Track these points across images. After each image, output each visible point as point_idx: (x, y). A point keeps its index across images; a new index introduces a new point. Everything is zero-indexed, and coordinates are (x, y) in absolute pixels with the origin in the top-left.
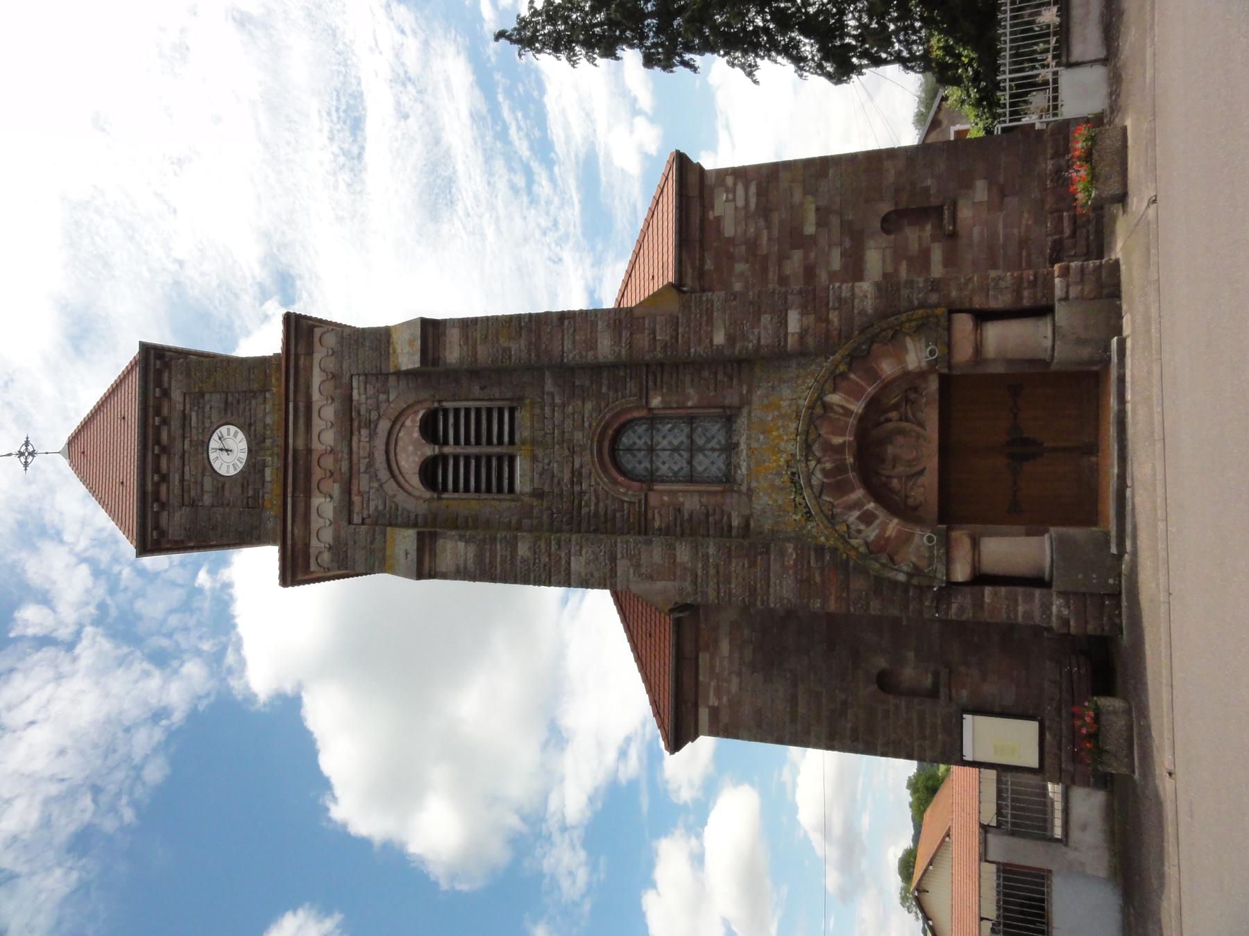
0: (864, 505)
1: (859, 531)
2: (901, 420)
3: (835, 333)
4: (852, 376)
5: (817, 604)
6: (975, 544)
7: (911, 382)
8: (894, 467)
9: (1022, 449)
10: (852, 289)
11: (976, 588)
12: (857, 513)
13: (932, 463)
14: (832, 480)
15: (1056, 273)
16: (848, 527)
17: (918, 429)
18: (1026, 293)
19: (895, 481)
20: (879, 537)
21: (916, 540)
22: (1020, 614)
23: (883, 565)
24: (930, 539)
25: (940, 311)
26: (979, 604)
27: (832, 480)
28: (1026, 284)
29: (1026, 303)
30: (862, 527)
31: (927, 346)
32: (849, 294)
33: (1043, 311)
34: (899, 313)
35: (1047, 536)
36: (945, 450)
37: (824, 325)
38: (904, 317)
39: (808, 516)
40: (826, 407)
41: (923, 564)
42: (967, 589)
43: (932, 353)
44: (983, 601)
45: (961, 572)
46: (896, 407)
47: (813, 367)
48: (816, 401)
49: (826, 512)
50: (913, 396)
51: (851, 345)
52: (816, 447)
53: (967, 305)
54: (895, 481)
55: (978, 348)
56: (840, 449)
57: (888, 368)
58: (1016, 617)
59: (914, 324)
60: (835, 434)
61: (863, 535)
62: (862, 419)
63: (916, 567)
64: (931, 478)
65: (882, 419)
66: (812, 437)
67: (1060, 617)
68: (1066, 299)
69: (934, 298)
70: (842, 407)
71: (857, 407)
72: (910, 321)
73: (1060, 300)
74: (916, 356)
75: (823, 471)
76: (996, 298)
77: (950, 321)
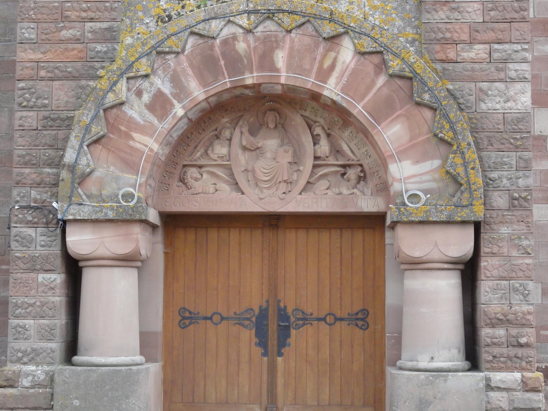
0: (177, 96)
1: (139, 93)
2: (316, 158)
3: (452, 55)
4: (381, 80)
5: (26, 31)
6: (126, 260)
7: (368, 172)
8: (245, 149)
9: (273, 328)
10: (523, 79)
11: (59, 262)
12: (167, 89)
13: (250, 203)
14: (217, 50)
15: (529, 375)
16: (147, 76)
17: (302, 183)
18: (501, 332)
19: (224, 151)
20: (131, 121)
21: (130, 177)
22: (21, 322)
23: (87, 129)
24: (128, 196)
25: (478, 212)
26: (34, 266)
27: (217, 50)
28: (514, 331)
29: (485, 333)
30: (146, 98)
31: (426, 192)
32: (513, 74)
33: (472, 357)
34: (479, 149)
35: (139, 358)
36: (273, 221)
37: (465, 37)
38: (472, 155)
39: (165, 19)
40: (333, 39)
41: (91, 186)
42: (57, 250)
43: (414, 197)
44: (38, 271)
45: (79, 241)
46: (337, 151)
47: (399, 23)
48: (342, 25)
49: (168, 43)
50: (352, 173)
51: (430, 77)
52: (270, 25)
53: (484, 249)
54: (224, 151)
55: (416, 264)
56: (266, 61)
57: (392, 134)
58: (17, 317)
59: (461, 170)
60: (290, 57)
61: (133, 97)
62: (316, 97)
63: (85, 177)
64: (226, 201)
65: (318, 130)
66: (287, 20)
67: (18, 374)
68: (489, 387)
69: (500, 200)
70: (332, 67)
71: (332, 90)
72: (465, 165)
73: (488, 380)
74: (411, 175)
75: (235, 38)
76: (495, 290)
77: (464, 223)
